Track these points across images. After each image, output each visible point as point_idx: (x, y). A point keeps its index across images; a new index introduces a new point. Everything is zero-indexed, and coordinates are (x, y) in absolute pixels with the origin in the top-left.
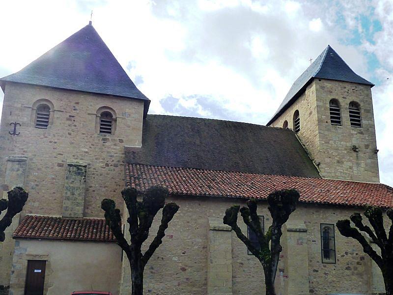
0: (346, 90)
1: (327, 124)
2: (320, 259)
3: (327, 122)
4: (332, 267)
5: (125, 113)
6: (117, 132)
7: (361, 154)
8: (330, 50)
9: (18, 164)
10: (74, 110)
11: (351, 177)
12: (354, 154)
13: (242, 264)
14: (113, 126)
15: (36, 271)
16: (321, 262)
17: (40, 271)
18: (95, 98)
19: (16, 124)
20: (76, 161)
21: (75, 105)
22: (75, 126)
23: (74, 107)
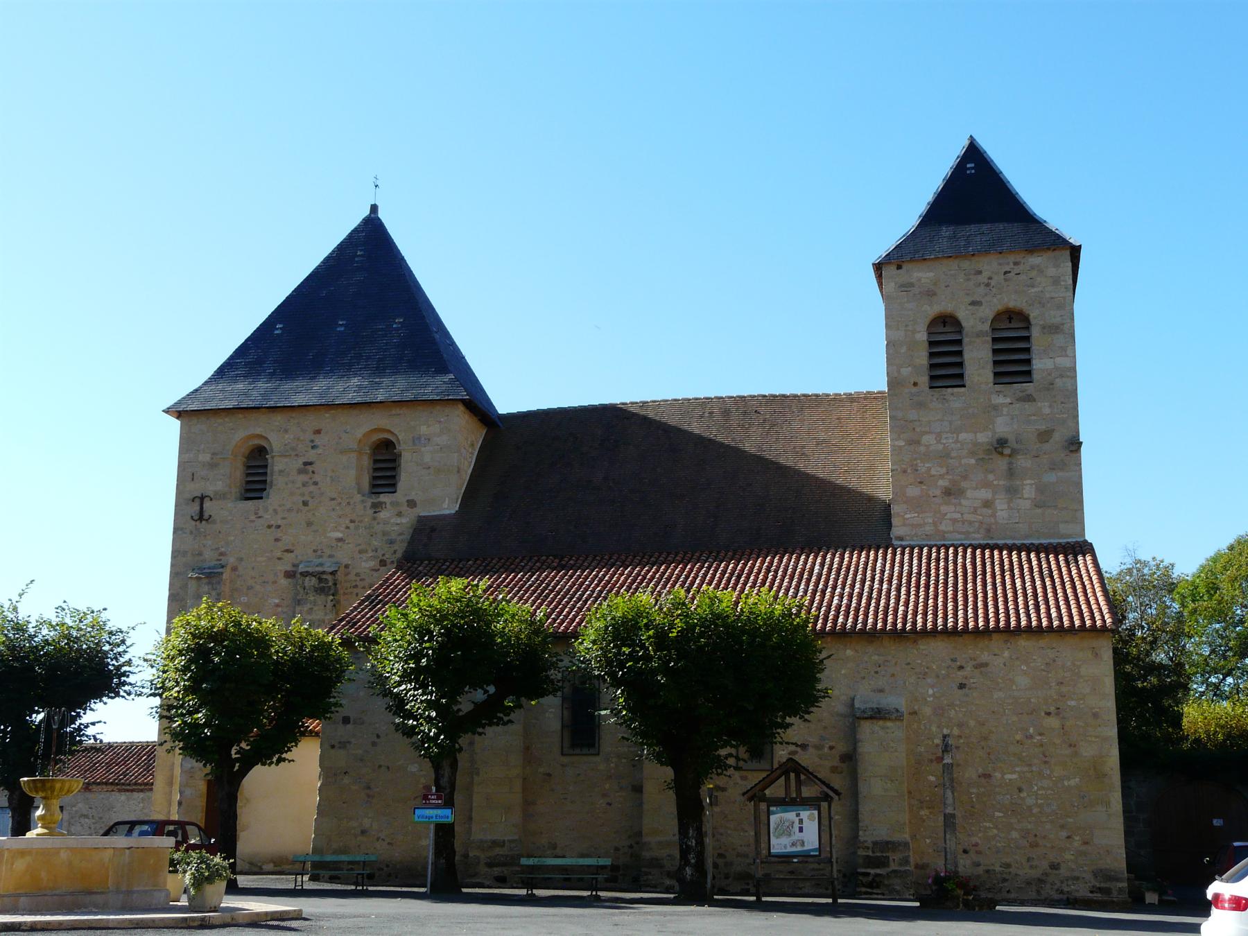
0: (982, 279)
1: (914, 390)
3: (915, 384)
6: (401, 486)
7: (1023, 462)
8: (973, 153)
10: (313, 447)
11: (988, 531)
12: (1001, 464)
13: (549, 775)
18: (355, 412)
19: (202, 498)
21: (313, 437)
22: (316, 483)
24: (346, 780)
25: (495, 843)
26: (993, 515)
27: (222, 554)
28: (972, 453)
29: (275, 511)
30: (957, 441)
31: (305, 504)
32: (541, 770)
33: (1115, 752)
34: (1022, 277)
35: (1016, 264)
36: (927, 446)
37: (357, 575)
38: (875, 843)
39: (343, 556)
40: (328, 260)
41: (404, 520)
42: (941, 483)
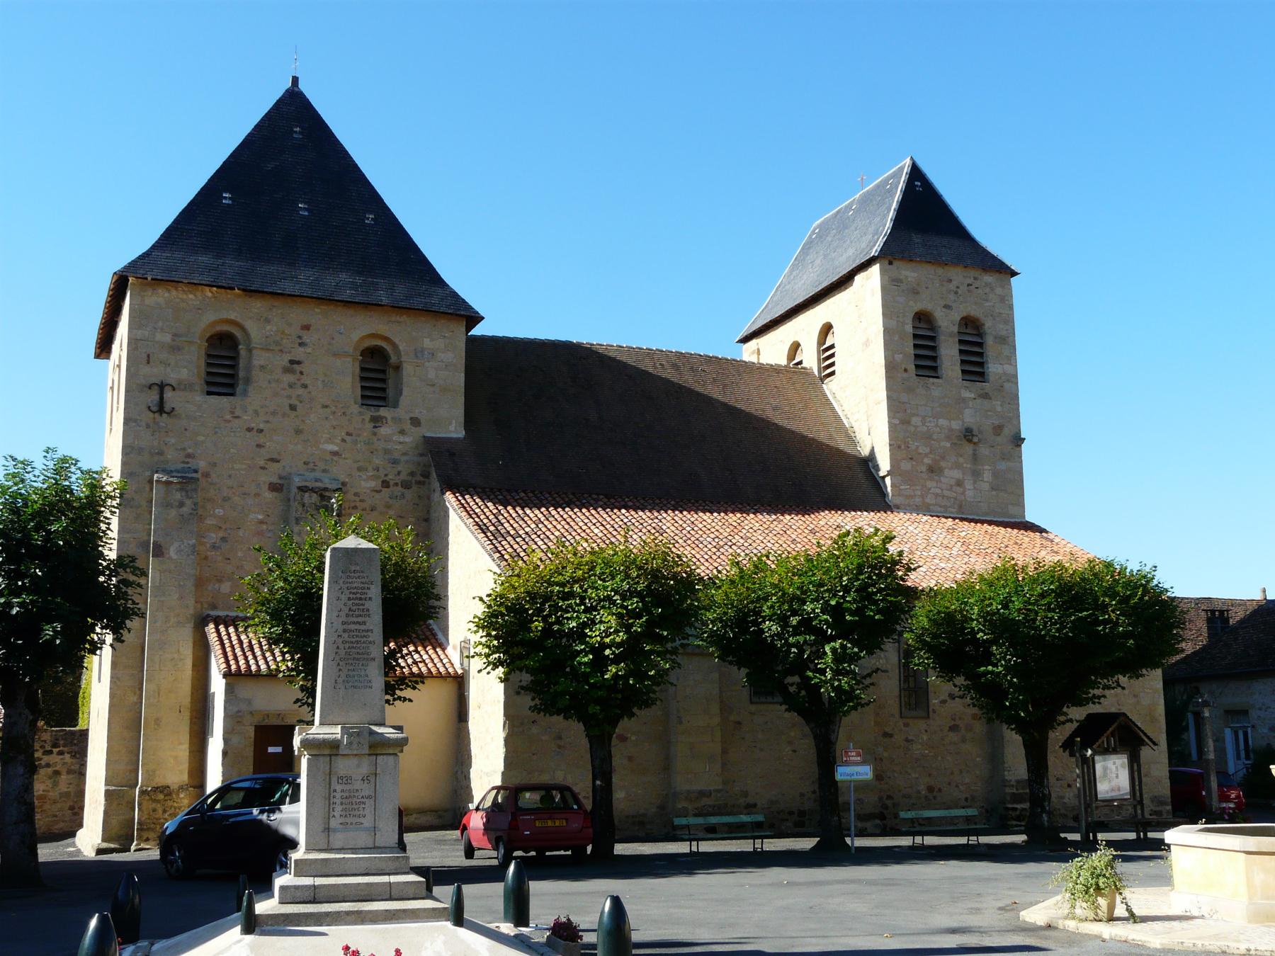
0: (952, 286)
1: (905, 375)
2: (896, 711)
4: (922, 724)
5: (423, 350)
6: (404, 400)
7: (984, 450)
8: (916, 173)
9: (181, 490)
10: (301, 344)
11: (960, 507)
12: (969, 449)
13: (739, 723)
14: (390, 382)
15: (271, 750)
16: (897, 715)
17: (279, 749)
19: (162, 387)
20: (312, 475)
22: (305, 386)
23: (300, 337)
24: (535, 730)
25: (702, 794)
26: (963, 493)
27: (189, 456)
28: (948, 438)
29: (256, 412)
30: (937, 426)
31: (293, 408)
32: (732, 718)
33: (1162, 701)
34: (980, 291)
35: (975, 279)
36: (916, 427)
37: (356, 494)
38: (1018, 782)
39: (340, 471)
40: (258, 127)
41: (407, 439)
42: (926, 461)
